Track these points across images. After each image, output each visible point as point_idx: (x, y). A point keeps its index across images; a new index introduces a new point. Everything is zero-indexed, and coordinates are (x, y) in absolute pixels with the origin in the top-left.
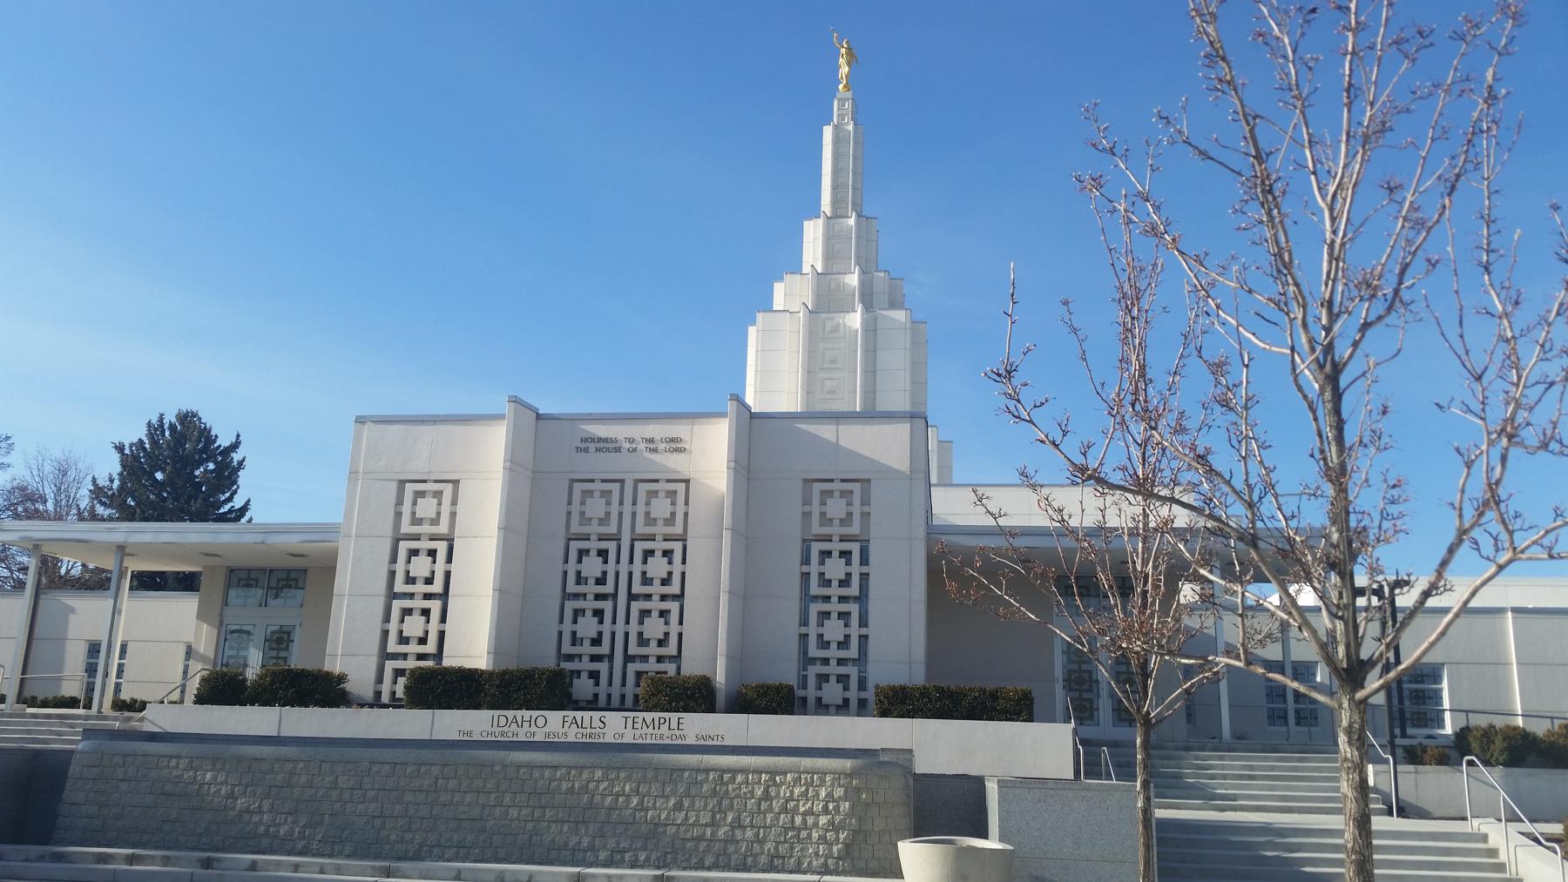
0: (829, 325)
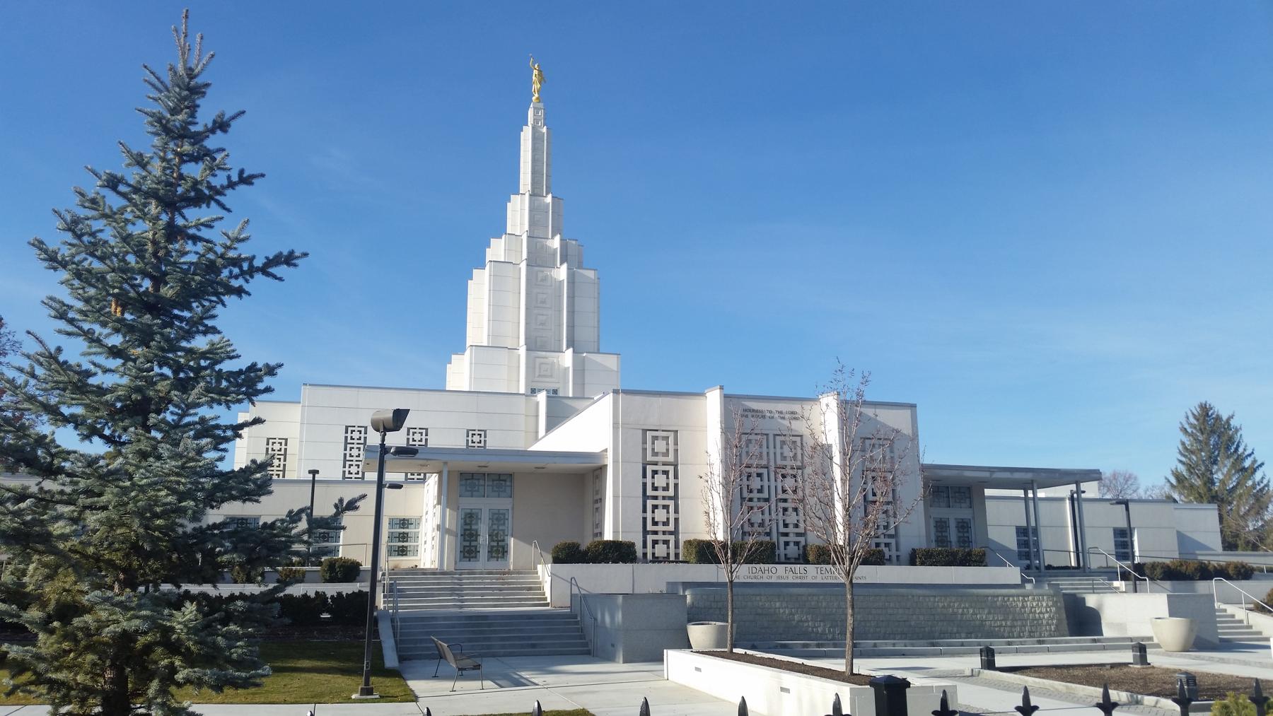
0: (540, 275)
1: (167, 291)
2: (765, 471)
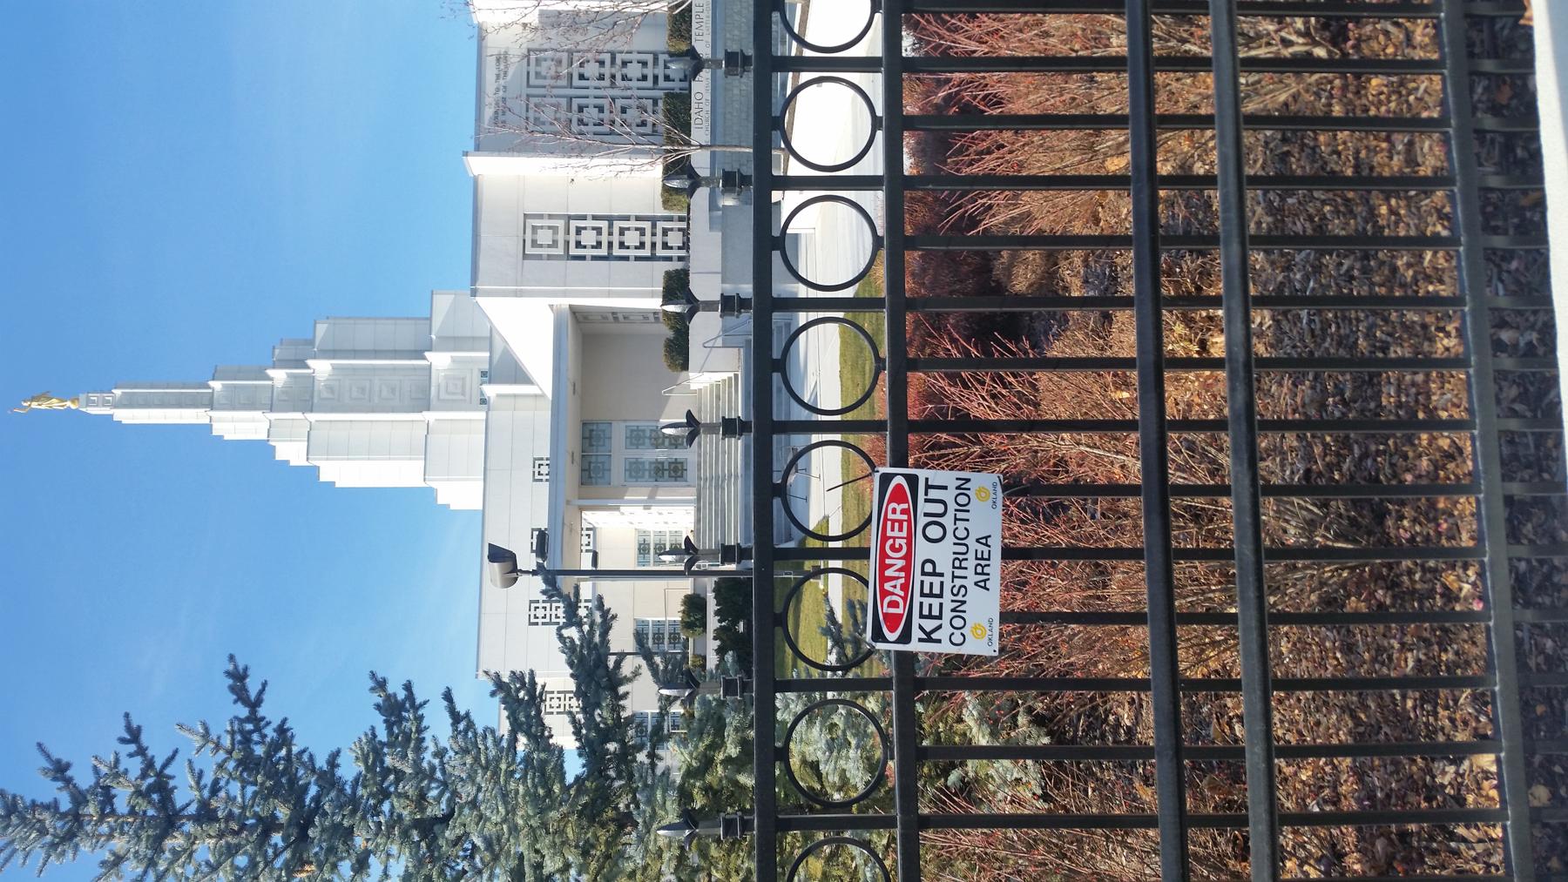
0: (325, 395)
1: (283, 813)
2: (576, 102)
